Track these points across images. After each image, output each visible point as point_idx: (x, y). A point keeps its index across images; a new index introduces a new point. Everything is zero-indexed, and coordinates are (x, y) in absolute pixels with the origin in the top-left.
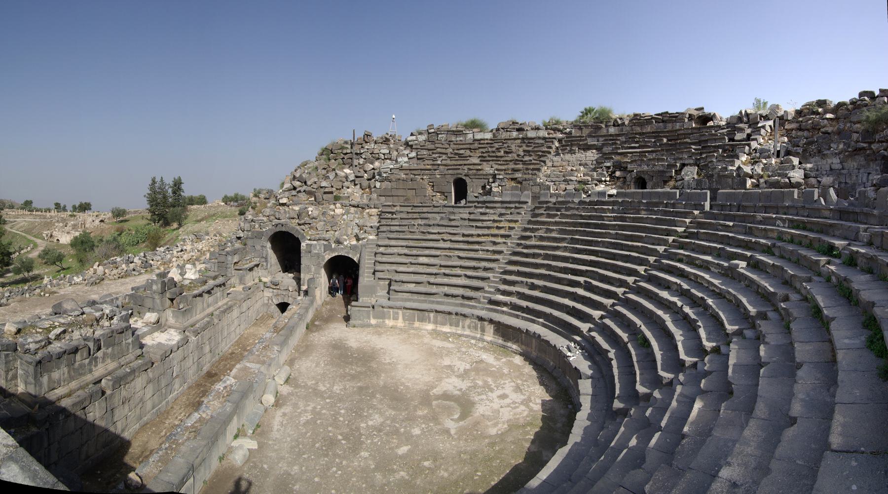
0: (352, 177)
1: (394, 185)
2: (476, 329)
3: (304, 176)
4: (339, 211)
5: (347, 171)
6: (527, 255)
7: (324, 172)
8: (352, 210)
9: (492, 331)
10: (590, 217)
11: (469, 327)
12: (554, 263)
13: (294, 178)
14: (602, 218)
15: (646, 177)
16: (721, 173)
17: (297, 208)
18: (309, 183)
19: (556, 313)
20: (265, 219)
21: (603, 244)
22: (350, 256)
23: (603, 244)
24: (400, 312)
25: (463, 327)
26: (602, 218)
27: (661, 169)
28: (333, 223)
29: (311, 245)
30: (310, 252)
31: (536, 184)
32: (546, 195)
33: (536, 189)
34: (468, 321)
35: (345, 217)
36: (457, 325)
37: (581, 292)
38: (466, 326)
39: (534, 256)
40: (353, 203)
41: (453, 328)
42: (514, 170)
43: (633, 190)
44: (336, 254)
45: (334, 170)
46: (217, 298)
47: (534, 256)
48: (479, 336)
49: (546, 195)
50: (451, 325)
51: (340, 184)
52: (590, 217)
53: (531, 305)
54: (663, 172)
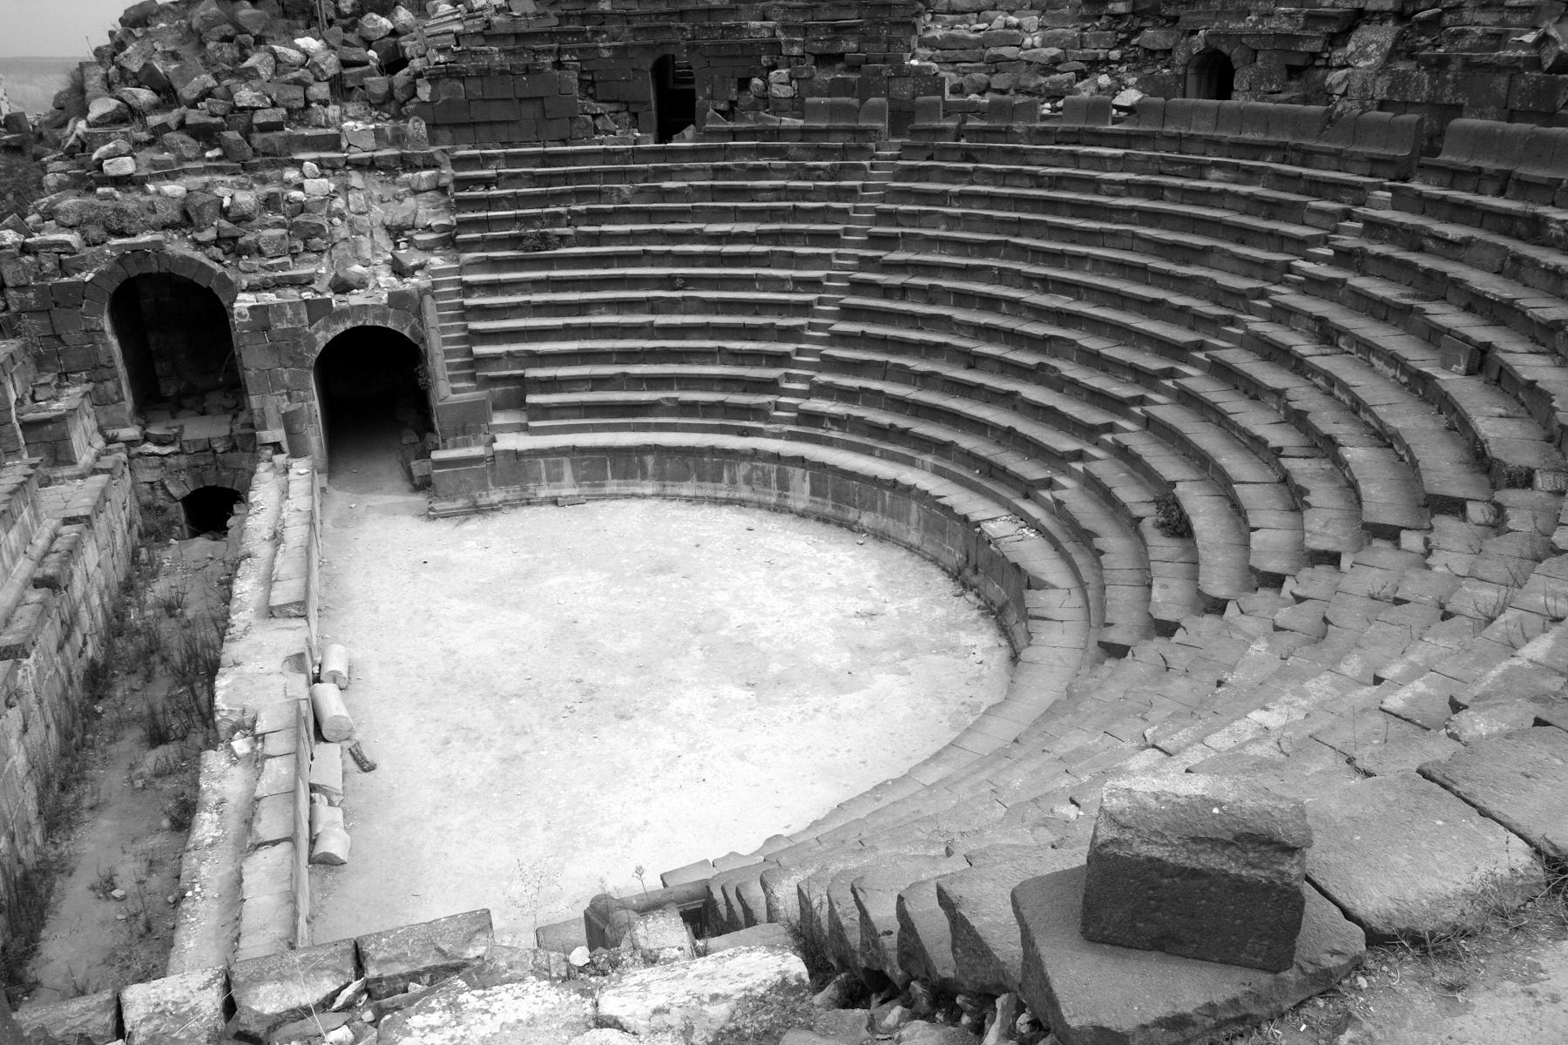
0: (330, 64)
1: (475, 88)
2: (767, 484)
3: (159, 66)
4: (319, 186)
5: (309, 43)
6: (887, 292)
7: (229, 51)
8: (356, 179)
9: (807, 487)
10: (1057, 182)
11: (748, 481)
12: (960, 315)
13: (125, 76)
14: (1094, 185)
15: (1236, 54)
16: (1477, 56)
17: (174, 189)
18: (187, 91)
19: (967, 442)
20: (73, 238)
21: (1099, 264)
22: (391, 325)
23: (1099, 264)
24: (566, 460)
25: (733, 482)
26: (1094, 185)
27: (1286, 27)
28: (307, 234)
29: (264, 309)
30: (267, 328)
31: (903, 73)
32: (930, 110)
33: (904, 90)
34: (743, 469)
35: (339, 203)
36: (717, 478)
37: (1032, 392)
38: (740, 478)
39: (903, 292)
40: (356, 155)
41: (709, 484)
42: (839, 30)
43: (1191, 101)
44: (349, 325)
45: (259, 40)
46: (24, 526)
47: (903, 292)
48: (773, 500)
49: (930, 110)
50: (701, 479)
51: (298, 92)
52: (1057, 182)
53: (902, 422)
54: (1290, 37)
